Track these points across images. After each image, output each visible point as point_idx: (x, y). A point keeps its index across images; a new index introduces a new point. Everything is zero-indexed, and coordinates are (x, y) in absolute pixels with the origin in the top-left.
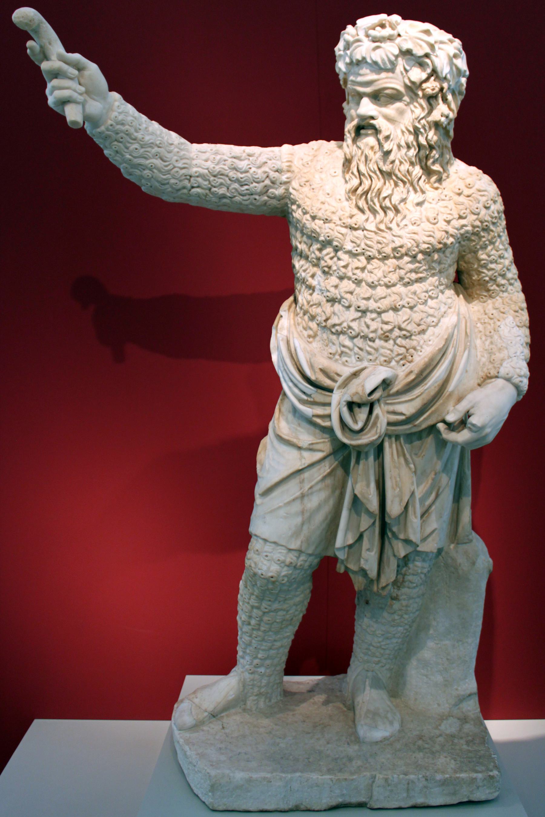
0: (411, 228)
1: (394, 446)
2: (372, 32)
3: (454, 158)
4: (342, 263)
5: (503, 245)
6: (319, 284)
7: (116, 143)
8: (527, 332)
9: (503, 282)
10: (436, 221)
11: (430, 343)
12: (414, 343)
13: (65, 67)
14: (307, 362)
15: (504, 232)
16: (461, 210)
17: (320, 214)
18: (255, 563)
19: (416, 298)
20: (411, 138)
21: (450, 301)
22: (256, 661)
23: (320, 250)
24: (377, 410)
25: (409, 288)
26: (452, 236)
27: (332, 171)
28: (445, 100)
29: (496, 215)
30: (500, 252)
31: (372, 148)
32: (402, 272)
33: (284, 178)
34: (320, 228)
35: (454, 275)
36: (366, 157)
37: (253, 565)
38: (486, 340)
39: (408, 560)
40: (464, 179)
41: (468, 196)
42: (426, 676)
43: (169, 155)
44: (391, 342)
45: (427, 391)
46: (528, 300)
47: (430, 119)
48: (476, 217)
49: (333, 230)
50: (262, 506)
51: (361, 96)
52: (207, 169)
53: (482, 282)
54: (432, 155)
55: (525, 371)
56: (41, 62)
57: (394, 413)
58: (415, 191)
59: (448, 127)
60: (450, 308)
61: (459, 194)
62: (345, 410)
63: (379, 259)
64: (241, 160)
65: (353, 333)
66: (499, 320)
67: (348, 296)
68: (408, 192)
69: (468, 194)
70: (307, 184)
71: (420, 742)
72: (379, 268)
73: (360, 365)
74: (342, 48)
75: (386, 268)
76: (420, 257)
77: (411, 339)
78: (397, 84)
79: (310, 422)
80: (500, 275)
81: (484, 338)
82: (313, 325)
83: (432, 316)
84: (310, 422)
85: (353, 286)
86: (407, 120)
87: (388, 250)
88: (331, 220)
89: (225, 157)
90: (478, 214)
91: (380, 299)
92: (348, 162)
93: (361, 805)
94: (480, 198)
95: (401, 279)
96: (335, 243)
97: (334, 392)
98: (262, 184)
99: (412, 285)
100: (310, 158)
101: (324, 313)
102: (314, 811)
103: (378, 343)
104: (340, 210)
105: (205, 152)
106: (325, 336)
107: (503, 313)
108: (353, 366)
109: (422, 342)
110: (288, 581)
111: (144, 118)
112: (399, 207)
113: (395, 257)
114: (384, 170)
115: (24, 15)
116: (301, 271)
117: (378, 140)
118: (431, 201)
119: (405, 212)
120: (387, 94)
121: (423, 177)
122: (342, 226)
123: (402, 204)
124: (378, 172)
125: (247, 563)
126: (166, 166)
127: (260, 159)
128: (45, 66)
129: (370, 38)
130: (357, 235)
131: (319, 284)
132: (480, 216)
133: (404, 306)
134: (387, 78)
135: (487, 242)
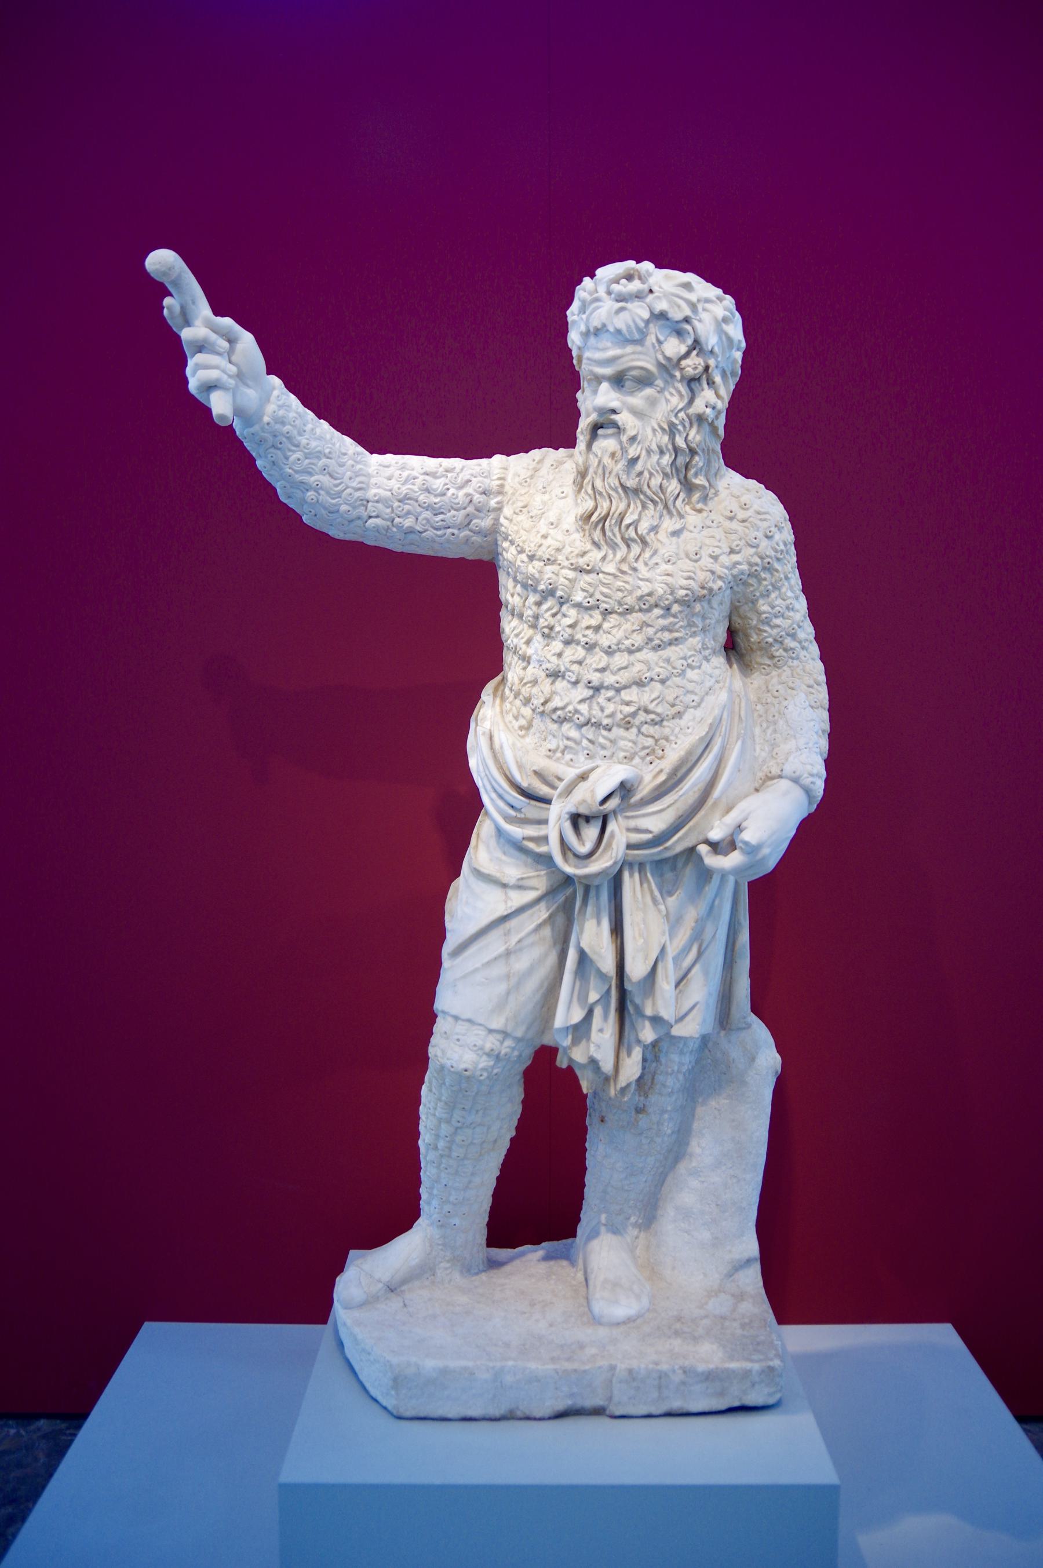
0: (664, 567)
1: (637, 875)
3: (725, 467)
4: (569, 621)
5: (793, 591)
7: (272, 450)
8: (826, 715)
9: (793, 644)
12: (667, 731)
13: (213, 337)
15: (794, 572)
16: (734, 541)
17: (539, 553)
18: (443, 1051)
19: (670, 668)
21: (717, 672)
22: (447, 1208)
23: (539, 604)
24: (612, 826)
25: (660, 653)
26: (720, 577)
27: (558, 491)
28: (711, 383)
30: (788, 602)
32: (650, 631)
33: (493, 503)
34: (540, 572)
35: (725, 635)
37: (439, 1054)
38: (768, 728)
40: (738, 497)
41: (743, 521)
42: (687, 1232)
43: (341, 470)
44: (634, 730)
47: (691, 411)
48: (754, 550)
49: (557, 575)
50: (451, 969)
51: (598, 379)
52: (390, 490)
53: (763, 644)
54: (694, 462)
55: (820, 769)
56: (183, 328)
57: (637, 830)
58: (669, 512)
59: (716, 423)
60: (717, 682)
62: (568, 826)
63: (620, 614)
65: (582, 719)
67: (575, 667)
68: (661, 516)
69: (748, 521)
71: (678, 1326)
73: (587, 765)
74: (576, 312)
75: (627, 626)
76: (676, 608)
77: (661, 726)
78: (648, 362)
79: (518, 847)
80: (788, 635)
81: (765, 725)
82: (527, 711)
83: (692, 692)
84: (518, 847)
86: (661, 413)
87: (630, 600)
88: (555, 561)
89: (415, 473)
90: (757, 546)
91: (620, 669)
92: (583, 474)
93: (598, 1412)
94: (759, 523)
95: (650, 640)
96: (559, 593)
98: (463, 512)
100: (529, 474)
102: (535, 1419)
103: (617, 732)
104: (567, 546)
105: (388, 467)
108: (584, 765)
109: (677, 730)
110: (488, 1077)
111: (310, 415)
112: (648, 539)
113: (641, 610)
115: (162, 261)
117: (621, 443)
118: (691, 528)
119: (656, 545)
120: (633, 377)
121: (682, 496)
122: (570, 569)
123: (652, 534)
124: (620, 490)
125: (432, 1051)
126: (336, 486)
127: (461, 475)
128: (186, 334)
130: (591, 581)
131: (536, 652)
132: (759, 549)
133: (652, 679)
134: (633, 353)
135: (770, 587)
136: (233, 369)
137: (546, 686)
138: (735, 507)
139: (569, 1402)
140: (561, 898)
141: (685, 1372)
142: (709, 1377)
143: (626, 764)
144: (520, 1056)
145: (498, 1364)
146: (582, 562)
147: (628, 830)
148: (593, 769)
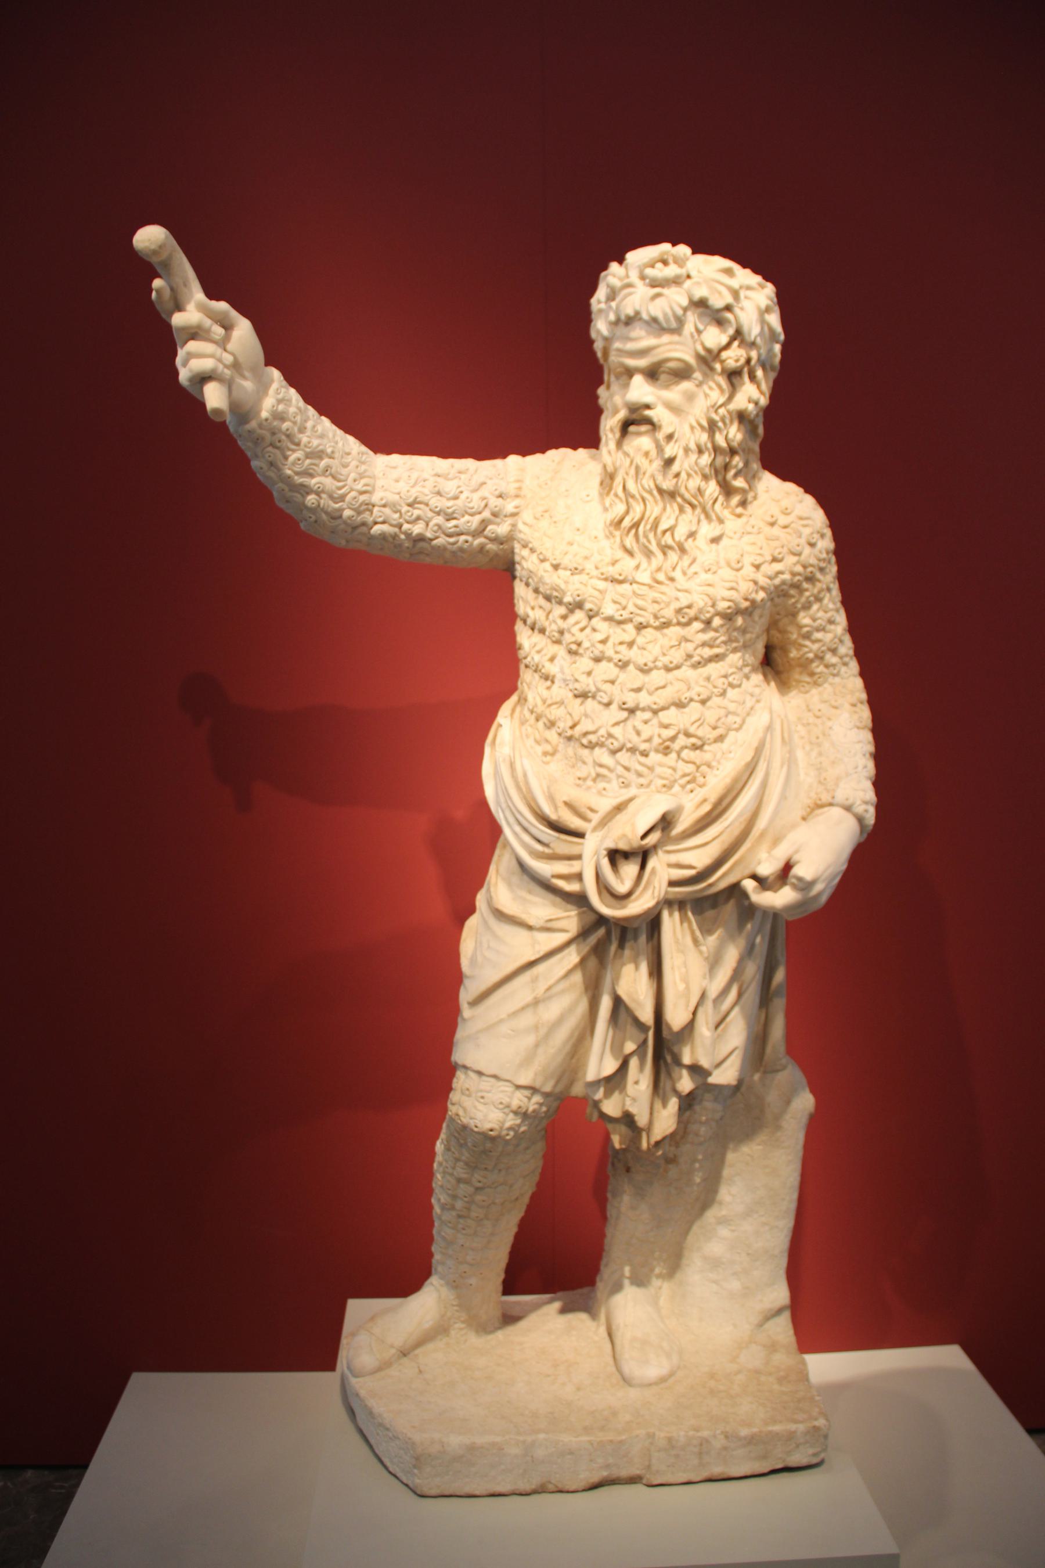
0: (704, 577)
1: (676, 914)
2: (649, 271)
3: (761, 470)
4: (599, 636)
5: (834, 603)
6: (562, 672)
7: (270, 449)
8: (868, 736)
9: (834, 660)
10: (740, 565)
11: (732, 755)
12: (707, 756)
13: (208, 322)
14: (544, 792)
16: (776, 548)
17: (566, 561)
19: (710, 686)
20: (704, 437)
21: (757, 691)
23: (564, 617)
24: (651, 863)
25: (700, 670)
26: (763, 588)
28: (752, 378)
29: (824, 555)
30: (830, 614)
31: (647, 454)
32: (690, 647)
33: (510, 507)
34: (566, 582)
36: (637, 468)
37: (461, 1113)
39: (694, 1099)
40: (778, 501)
41: (785, 527)
42: (715, 1282)
43: (344, 471)
44: (674, 755)
45: (729, 830)
46: (868, 687)
47: (732, 407)
49: (585, 585)
51: (630, 373)
52: (399, 494)
54: (734, 462)
55: (870, 795)
57: (679, 866)
58: (708, 517)
60: (758, 701)
61: (772, 524)
62: (605, 862)
63: (656, 628)
64: (449, 480)
65: (616, 745)
66: (829, 719)
67: (607, 687)
68: (699, 521)
69: (784, 525)
70: (546, 515)
71: (712, 1383)
72: (655, 641)
75: (666, 642)
76: (717, 622)
81: (808, 748)
82: (552, 735)
83: (734, 713)
85: (616, 671)
86: (699, 410)
87: (669, 613)
88: (583, 570)
89: (425, 475)
90: (799, 554)
91: (657, 689)
92: (609, 478)
93: (633, 1480)
95: (689, 656)
97: (587, 836)
98: (477, 519)
99: (704, 666)
101: (570, 715)
102: (568, 1492)
103: (654, 758)
105: (395, 468)
106: (570, 751)
107: (836, 708)
111: (311, 411)
113: (679, 624)
114: (665, 487)
115: (150, 237)
116: (533, 653)
117: (657, 442)
118: (731, 534)
120: (670, 369)
122: (600, 579)
123: (690, 540)
124: (655, 492)
126: (340, 488)
128: (178, 320)
129: (647, 281)
132: (803, 557)
133: (691, 700)
134: (670, 343)
136: (228, 359)
137: (576, 707)
138: (776, 511)
139: (605, 1473)
140: (593, 939)
141: (727, 1437)
142: (751, 1441)
143: (665, 792)
144: (548, 1111)
145: (529, 1439)
146: (612, 571)
147: (670, 866)
148: (631, 800)
